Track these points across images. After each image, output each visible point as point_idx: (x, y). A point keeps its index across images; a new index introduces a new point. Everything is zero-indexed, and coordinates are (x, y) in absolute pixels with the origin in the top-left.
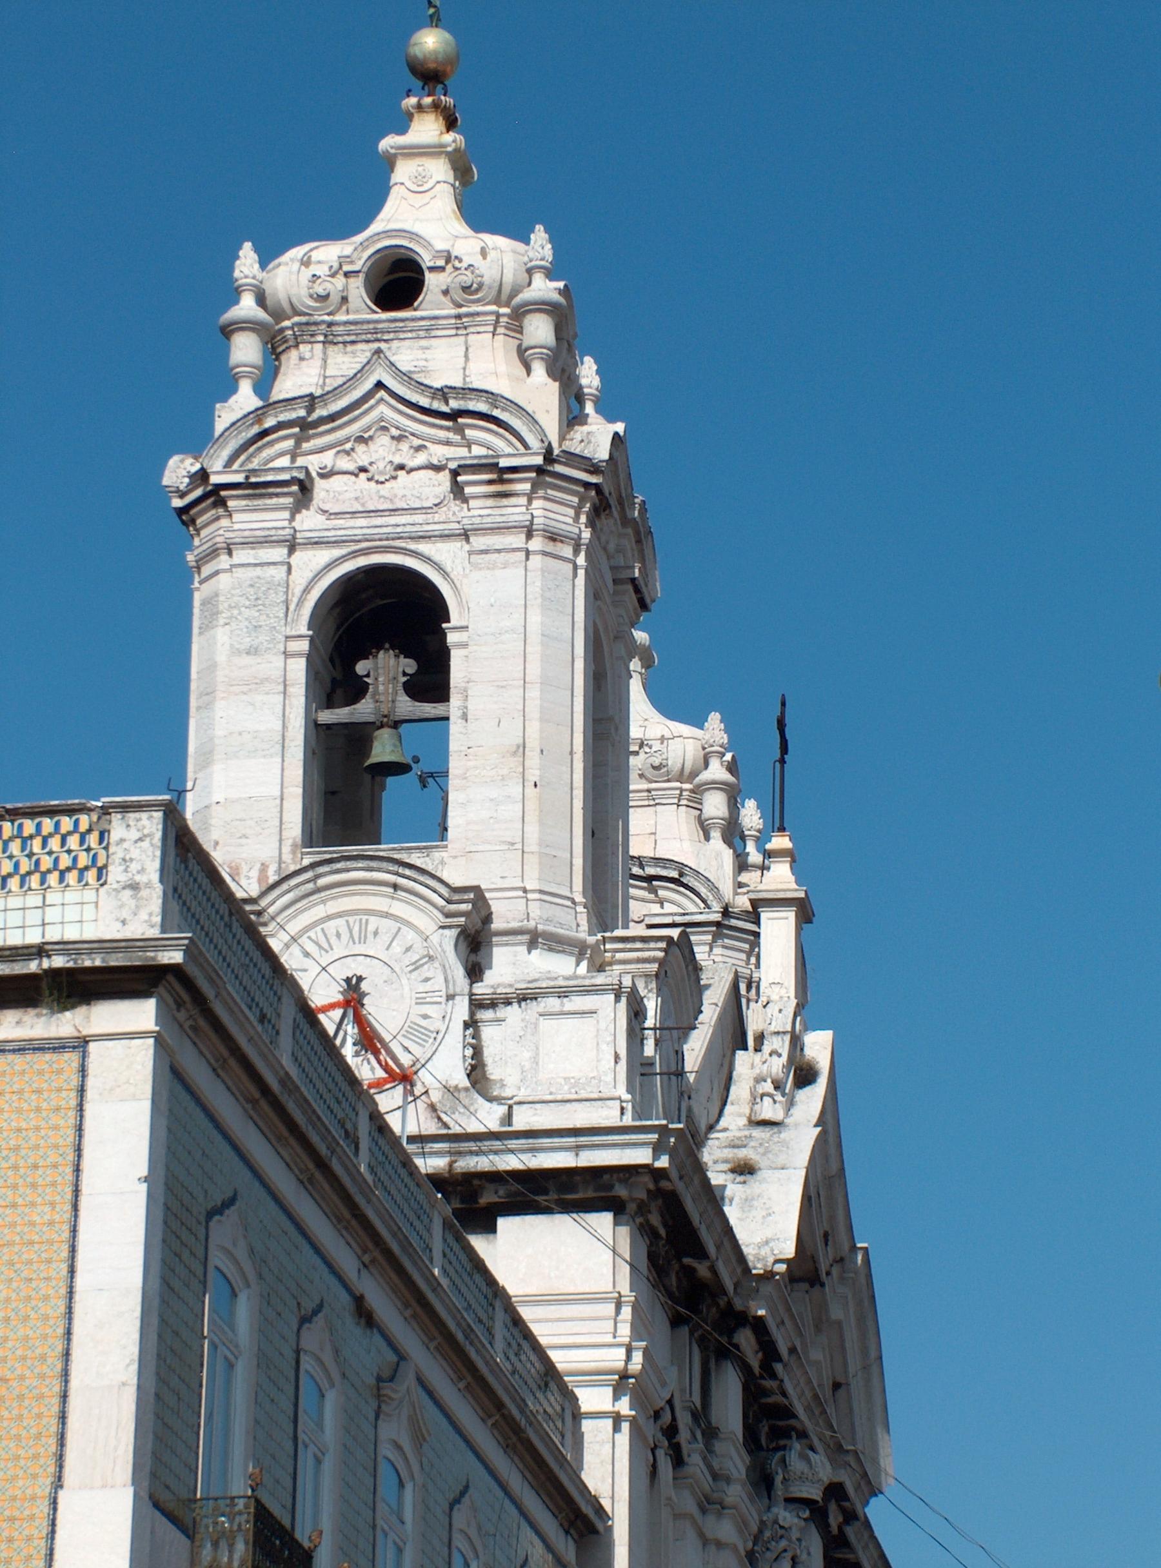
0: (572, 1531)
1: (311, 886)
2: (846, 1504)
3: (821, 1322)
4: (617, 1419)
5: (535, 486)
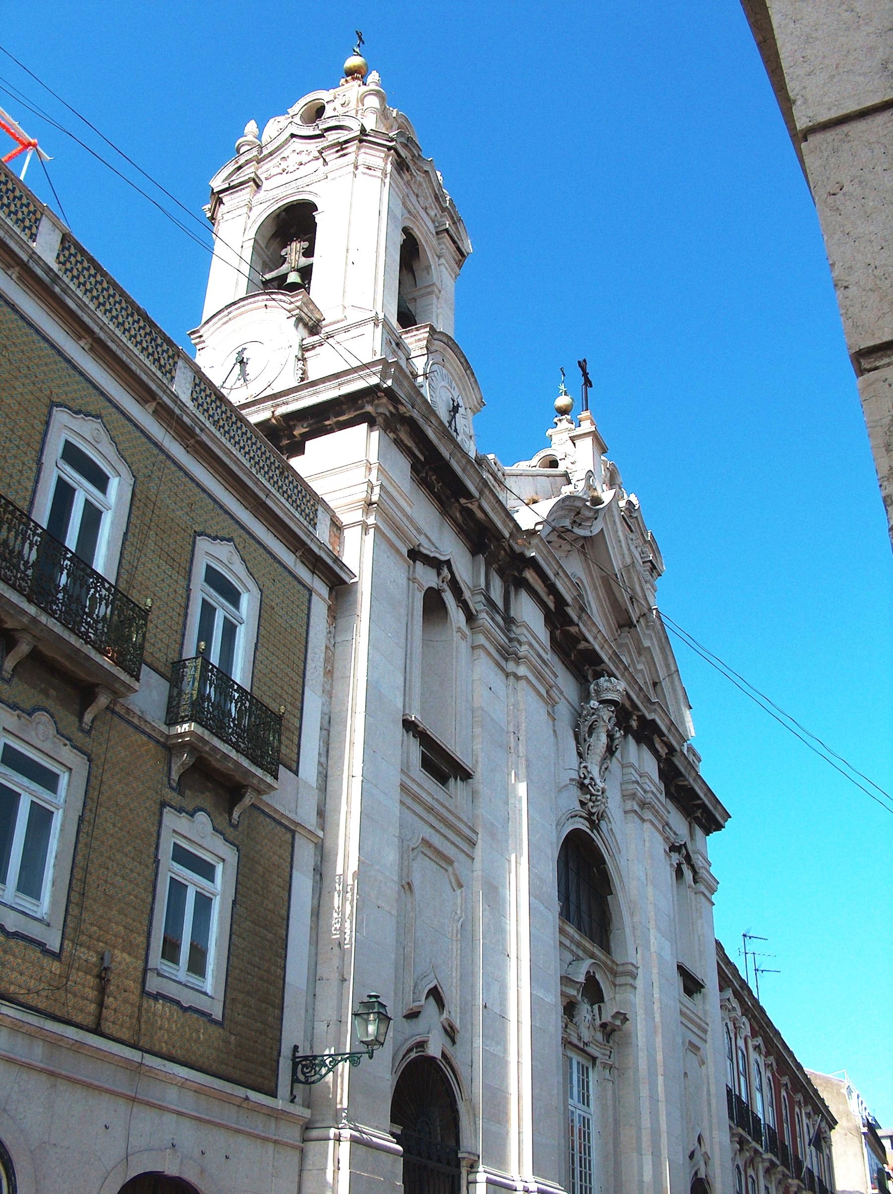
1: (227, 319)
3: (641, 650)
4: (365, 528)
5: (359, 148)
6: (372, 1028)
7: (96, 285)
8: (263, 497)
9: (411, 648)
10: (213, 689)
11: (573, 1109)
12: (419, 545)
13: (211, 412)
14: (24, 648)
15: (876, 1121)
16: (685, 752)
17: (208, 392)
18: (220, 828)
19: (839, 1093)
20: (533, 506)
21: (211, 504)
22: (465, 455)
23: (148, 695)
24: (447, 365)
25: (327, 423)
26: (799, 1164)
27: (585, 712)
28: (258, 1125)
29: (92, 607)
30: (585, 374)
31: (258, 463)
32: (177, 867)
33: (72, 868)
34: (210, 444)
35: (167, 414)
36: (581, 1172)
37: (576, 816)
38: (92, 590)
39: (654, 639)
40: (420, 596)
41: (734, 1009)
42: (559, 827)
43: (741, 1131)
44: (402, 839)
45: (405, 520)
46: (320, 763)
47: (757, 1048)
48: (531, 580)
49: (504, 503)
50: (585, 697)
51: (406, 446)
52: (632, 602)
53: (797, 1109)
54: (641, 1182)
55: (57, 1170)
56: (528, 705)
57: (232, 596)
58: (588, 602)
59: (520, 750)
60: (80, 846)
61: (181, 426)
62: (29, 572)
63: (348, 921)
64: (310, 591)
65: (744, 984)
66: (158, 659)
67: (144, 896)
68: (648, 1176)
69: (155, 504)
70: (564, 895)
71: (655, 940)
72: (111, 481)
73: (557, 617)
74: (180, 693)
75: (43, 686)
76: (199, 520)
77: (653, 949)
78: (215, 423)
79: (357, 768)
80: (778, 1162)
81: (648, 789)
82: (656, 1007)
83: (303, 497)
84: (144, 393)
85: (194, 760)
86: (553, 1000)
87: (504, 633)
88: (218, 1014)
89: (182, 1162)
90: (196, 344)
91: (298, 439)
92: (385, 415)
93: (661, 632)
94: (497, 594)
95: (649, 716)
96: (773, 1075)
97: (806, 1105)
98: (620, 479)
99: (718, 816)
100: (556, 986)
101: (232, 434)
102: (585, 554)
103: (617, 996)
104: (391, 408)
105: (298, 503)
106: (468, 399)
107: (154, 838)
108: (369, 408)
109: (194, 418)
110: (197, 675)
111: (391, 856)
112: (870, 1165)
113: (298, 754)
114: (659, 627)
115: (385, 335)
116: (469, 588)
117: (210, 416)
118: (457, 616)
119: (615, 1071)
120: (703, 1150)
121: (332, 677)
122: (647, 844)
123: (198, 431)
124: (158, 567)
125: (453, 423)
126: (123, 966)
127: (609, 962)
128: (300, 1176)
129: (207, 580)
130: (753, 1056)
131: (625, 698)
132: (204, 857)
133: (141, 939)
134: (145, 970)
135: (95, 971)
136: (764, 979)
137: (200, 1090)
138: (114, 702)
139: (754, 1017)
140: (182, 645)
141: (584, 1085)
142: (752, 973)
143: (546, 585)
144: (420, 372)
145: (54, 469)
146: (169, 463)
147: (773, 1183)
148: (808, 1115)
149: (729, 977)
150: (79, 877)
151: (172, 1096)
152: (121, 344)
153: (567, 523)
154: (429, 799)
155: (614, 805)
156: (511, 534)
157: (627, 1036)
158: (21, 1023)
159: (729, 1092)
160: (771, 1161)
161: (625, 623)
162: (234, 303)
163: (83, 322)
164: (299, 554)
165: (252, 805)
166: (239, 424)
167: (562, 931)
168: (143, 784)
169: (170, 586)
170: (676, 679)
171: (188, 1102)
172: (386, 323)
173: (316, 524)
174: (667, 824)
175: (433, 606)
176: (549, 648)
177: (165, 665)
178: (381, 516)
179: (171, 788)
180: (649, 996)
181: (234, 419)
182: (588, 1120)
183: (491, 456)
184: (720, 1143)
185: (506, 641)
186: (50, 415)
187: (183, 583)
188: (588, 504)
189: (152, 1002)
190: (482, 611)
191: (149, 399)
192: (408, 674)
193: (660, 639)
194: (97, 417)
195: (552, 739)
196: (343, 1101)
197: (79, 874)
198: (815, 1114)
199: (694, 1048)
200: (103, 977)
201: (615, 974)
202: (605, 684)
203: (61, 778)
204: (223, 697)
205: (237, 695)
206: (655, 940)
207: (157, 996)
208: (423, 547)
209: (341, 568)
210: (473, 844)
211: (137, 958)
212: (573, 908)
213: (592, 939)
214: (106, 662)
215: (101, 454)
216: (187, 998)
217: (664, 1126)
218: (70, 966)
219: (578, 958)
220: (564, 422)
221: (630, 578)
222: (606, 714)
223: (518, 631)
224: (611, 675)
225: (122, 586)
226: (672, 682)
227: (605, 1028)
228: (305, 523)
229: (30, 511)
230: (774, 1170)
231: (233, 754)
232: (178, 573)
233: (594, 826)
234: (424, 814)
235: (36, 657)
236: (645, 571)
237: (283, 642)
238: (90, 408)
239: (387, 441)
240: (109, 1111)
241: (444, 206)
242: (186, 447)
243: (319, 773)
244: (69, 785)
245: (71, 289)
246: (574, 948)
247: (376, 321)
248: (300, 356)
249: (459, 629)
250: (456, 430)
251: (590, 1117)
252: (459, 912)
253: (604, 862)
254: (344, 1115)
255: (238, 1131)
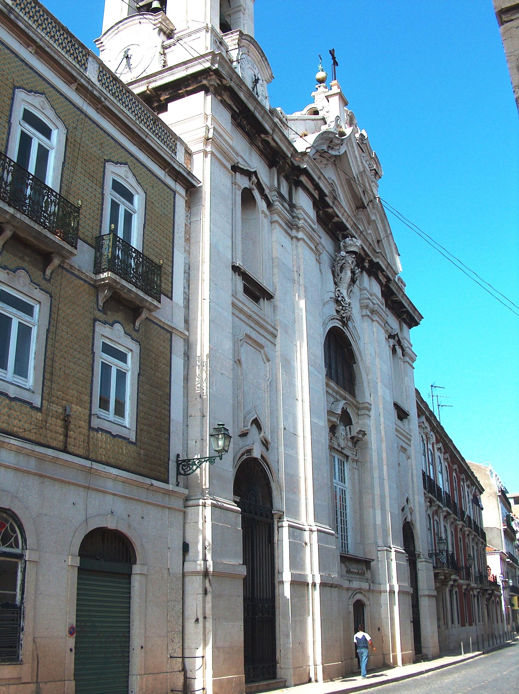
0: (178, 181)
1: (117, 31)
2: (384, 273)
3: (370, 222)
4: (206, 153)
6: (221, 443)
7: (36, 13)
8: (144, 137)
9: (235, 224)
10: (120, 252)
11: (336, 485)
12: (238, 162)
13: (110, 88)
14: (8, 233)
15: (506, 489)
16: (397, 281)
17: (108, 76)
18: (128, 332)
19: (485, 474)
20: (304, 138)
21: (114, 143)
22: (263, 108)
23: (83, 257)
24: (250, 54)
25: (180, 92)
26: (463, 513)
27: (338, 259)
28: (159, 499)
29: (47, 207)
30: (334, 58)
31: (140, 117)
32: (105, 356)
33: (45, 359)
34: (111, 107)
35: (84, 90)
36: (341, 519)
37: (334, 319)
38: (46, 197)
39: (378, 215)
40: (239, 193)
41: (426, 427)
42: (325, 326)
43: (430, 495)
44: (234, 332)
45: (228, 148)
46: (185, 293)
47: (439, 449)
48: (304, 182)
49: (287, 136)
50: (338, 249)
51: (227, 104)
53: (462, 483)
54: (375, 525)
55: (48, 528)
56: (304, 255)
57: (129, 197)
58: (339, 194)
59: (301, 281)
60: (48, 346)
61: (93, 97)
62: (8, 188)
63: (205, 382)
64: (174, 192)
65: (432, 414)
66: (87, 236)
67: (86, 373)
68: (379, 521)
69: (80, 144)
70: (328, 365)
71: (381, 389)
72: (53, 132)
73: (320, 203)
74: (101, 255)
75: (20, 255)
76: (106, 152)
77: (379, 394)
78: (113, 94)
79: (207, 295)
80: (451, 512)
81: (375, 302)
82: (382, 427)
83: (168, 136)
84: (70, 78)
85: (111, 293)
86: (323, 423)
87: (289, 213)
88: (133, 438)
89: (117, 521)
90: (99, 48)
91: (163, 102)
92: (215, 85)
93: (381, 211)
94: (284, 191)
95: (375, 260)
96: (448, 464)
97: (467, 481)
98: (355, 121)
99: (416, 318)
100: (324, 415)
101: (124, 100)
102: (335, 165)
103: (360, 422)
104: (218, 82)
105: (165, 140)
106: (264, 75)
107: (91, 340)
108: (205, 82)
109: (100, 92)
110: (111, 244)
111: (228, 345)
112: (503, 513)
113: (172, 288)
114: (381, 208)
115: (213, 37)
116: (268, 188)
117: (110, 90)
118: (261, 204)
119: (360, 463)
120: (409, 506)
121: (190, 242)
122: (375, 334)
123: (103, 99)
124: (84, 182)
125: (255, 88)
126: (78, 414)
127: (355, 402)
128: (184, 526)
129: (113, 188)
130: (437, 453)
131: (361, 249)
132: (120, 349)
133: (87, 398)
134: (90, 415)
135: (62, 417)
136: (443, 410)
137: (125, 481)
138: (63, 262)
139: (438, 432)
140: (101, 226)
141: (342, 471)
142: (436, 407)
143: (313, 185)
144: (235, 59)
145: (19, 127)
146: (87, 119)
147: (449, 524)
148: (468, 486)
149: (423, 409)
150: (49, 364)
151: (110, 485)
152: (54, 49)
153: (325, 147)
154: (249, 311)
155: (356, 312)
156: (292, 155)
157: (366, 443)
158: (21, 449)
159: (424, 474)
160: (448, 512)
161: (361, 206)
162: (121, 22)
163: (30, 36)
164: (167, 170)
165: (147, 318)
166: (127, 94)
167: (327, 385)
168: (83, 309)
169: (91, 193)
171: (119, 488)
172: (213, 30)
173: (176, 152)
174: (387, 323)
175: (247, 199)
176: (316, 221)
177: (92, 239)
178: (214, 146)
179: (99, 310)
180: (378, 422)
181: (124, 92)
182: (345, 491)
183: (279, 109)
184: (419, 502)
185: (291, 218)
186: (14, 94)
187: (100, 190)
188: (337, 136)
189: (95, 433)
190: (276, 201)
191: (73, 81)
192: (234, 239)
193: (381, 214)
194: (42, 94)
195: (319, 275)
196: (206, 484)
197: (49, 362)
198: (472, 485)
199: (404, 450)
200: (66, 420)
201: (358, 409)
202: (349, 242)
203: (35, 307)
204: (126, 256)
205: (134, 255)
206: (381, 389)
207: (98, 430)
208: (240, 164)
209: (192, 178)
210: (275, 336)
211: (85, 409)
212: (333, 371)
213: (345, 389)
214: (57, 239)
215: (46, 116)
216: (115, 430)
217: (387, 493)
218: (47, 415)
219: (337, 400)
220: (322, 88)
221: (363, 179)
222: (350, 259)
223: (298, 212)
224: (353, 236)
225: (63, 194)
226: (389, 240)
227: (353, 439)
228: (170, 152)
229: (6, 152)
230: (449, 517)
231: (134, 289)
232: (96, 185)
233: (345, 324)
234: (246, 320)
235: (15, 238)
236: (371, 175)
237: (160, 223)
238: (38, 89)
239: (216, 101)
240: (74, 495)
242: (97, 110)
243: (184, 298)
244: (40, 311)
245: (20, 16)
246: (334, 394)
247: (207, 29)
248: (162, 53)
249: (263, 212)
250: (257, 94)
251: (345, 489)
252: (268, 375)
253: (351, 345)
254: (207, 492)
255: (147, 503)
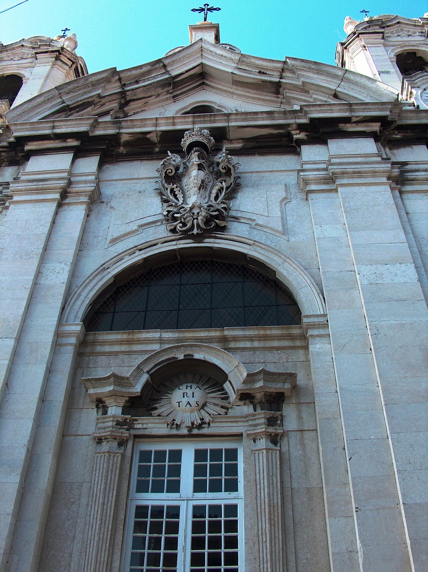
3: (304, 89)
52: (263, 73)
170: (352, 77)
193: (310, 68)
241: (421, 24)
253: (211, 248)
